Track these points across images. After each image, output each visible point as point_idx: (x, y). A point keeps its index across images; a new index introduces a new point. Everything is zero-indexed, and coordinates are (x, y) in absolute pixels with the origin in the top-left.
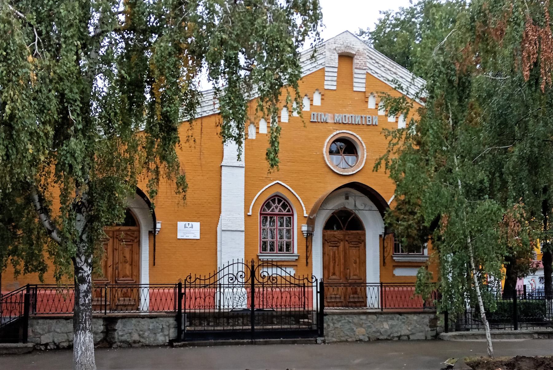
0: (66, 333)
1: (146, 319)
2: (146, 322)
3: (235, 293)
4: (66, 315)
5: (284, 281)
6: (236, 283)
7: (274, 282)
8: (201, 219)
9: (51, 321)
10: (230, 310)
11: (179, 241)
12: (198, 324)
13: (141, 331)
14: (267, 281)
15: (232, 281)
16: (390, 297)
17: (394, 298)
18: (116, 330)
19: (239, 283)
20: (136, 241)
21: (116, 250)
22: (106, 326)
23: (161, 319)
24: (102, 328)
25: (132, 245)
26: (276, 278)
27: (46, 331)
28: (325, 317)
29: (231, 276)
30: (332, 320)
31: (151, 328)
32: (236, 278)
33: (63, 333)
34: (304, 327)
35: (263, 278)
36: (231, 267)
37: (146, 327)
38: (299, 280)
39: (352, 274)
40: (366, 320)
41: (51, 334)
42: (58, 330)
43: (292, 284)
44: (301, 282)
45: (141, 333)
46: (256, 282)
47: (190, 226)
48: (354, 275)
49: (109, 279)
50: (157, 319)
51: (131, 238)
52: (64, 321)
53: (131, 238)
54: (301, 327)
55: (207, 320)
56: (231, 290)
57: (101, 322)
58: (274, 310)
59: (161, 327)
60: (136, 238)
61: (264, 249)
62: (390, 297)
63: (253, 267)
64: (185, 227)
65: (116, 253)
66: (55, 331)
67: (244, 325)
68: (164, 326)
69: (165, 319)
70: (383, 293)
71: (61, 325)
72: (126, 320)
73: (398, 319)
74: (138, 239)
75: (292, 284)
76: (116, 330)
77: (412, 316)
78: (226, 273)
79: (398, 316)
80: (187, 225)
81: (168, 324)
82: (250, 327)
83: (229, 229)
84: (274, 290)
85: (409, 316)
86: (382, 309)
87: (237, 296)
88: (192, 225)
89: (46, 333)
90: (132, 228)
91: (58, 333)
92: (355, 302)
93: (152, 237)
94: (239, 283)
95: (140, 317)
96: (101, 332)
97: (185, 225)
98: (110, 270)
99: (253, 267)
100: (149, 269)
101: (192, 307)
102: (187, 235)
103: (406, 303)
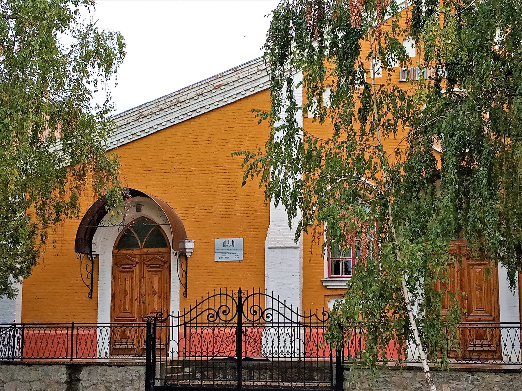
0: (29, 382)
1: (113, 367)
2: (113, 371)
3: (216, 335)
4: (29, 360)
5: (282, 319)
6: (218, 321)
7: (268, 320)
8: (244, 233)
9: (14, 367)
10: (210, 358)
11: (217, 264)
12: (211, 376)
13: (108, 382)
14: (259, 319)
15: (213, 319)
16: (83, 342)
17: (33, 344)
18: (81, 380)
19: (221, 321)
20: (166, 266)
21: (143, 278)
22: (69, 374)
23: (131, 368)
24: (65, 377)
25: (161, 271)
26: (272, 315)
27: (9, 378)
28: (345, 372)
29: (211, 311)
30: (359, 377)
31: (118, 379)
32: (217, 314)
33: (25, 381)
34: (260, 383)
35: (254, 315)
36: (211, 300)
37: (113, 378)
38: (304, 317)
39: (474, 308)
40: (413, 378)
41: (14, 382)
42: (21, 378)
43: (294, 323)
44: (307, 320)
45: (108, 385)
46: (244, 320)
47: (231, 243)
48: (478, 309)
49: (136, 316)
50: (125, 368)
51: (160, 263)
52: (27, 368)
53: (160, 263)
54: (256, 383)
55: (223, 372)
56: (210, 331)
57: (64, 370)
58: (267, 360)
59: (131, 378)
60: (166, 262)
61: (336, 271)
62: (83, 342)
63: (240, 299)
64: (225, 245)
65: (145, 282)
66: (18, 379)
67: (320, 380)
68: (134, 378)
69: (135, 368)
70: (75, 337)
71: (24, 371)
72: (91, 367)
73: (467, 380)
74: (168, 264)
75: (294, 323)
76: (81, 380)
77: (492, 375)
78: (205, 307)
79: (466, 375)
80: (227, 243)
81: (138, 375)
82: (236, 383)
83: (278, 245)
84: (205, 331)
85: (486, 376)
86: (71, 359)
87: (219, 340)
88: (233, 242)
89: (9, 382)
90: (162, 250)
91: (21, 381)
92: (479, 352)
93: (184, 261)
94: (221, 321)
95: (106, 365)
96: (64, 383)
97: (224, 243)
98: (136, 304)
99: (240, 299)
100: (180, 303)
101: (205, 354)
102: (227, 256)
103: (30, 352)
